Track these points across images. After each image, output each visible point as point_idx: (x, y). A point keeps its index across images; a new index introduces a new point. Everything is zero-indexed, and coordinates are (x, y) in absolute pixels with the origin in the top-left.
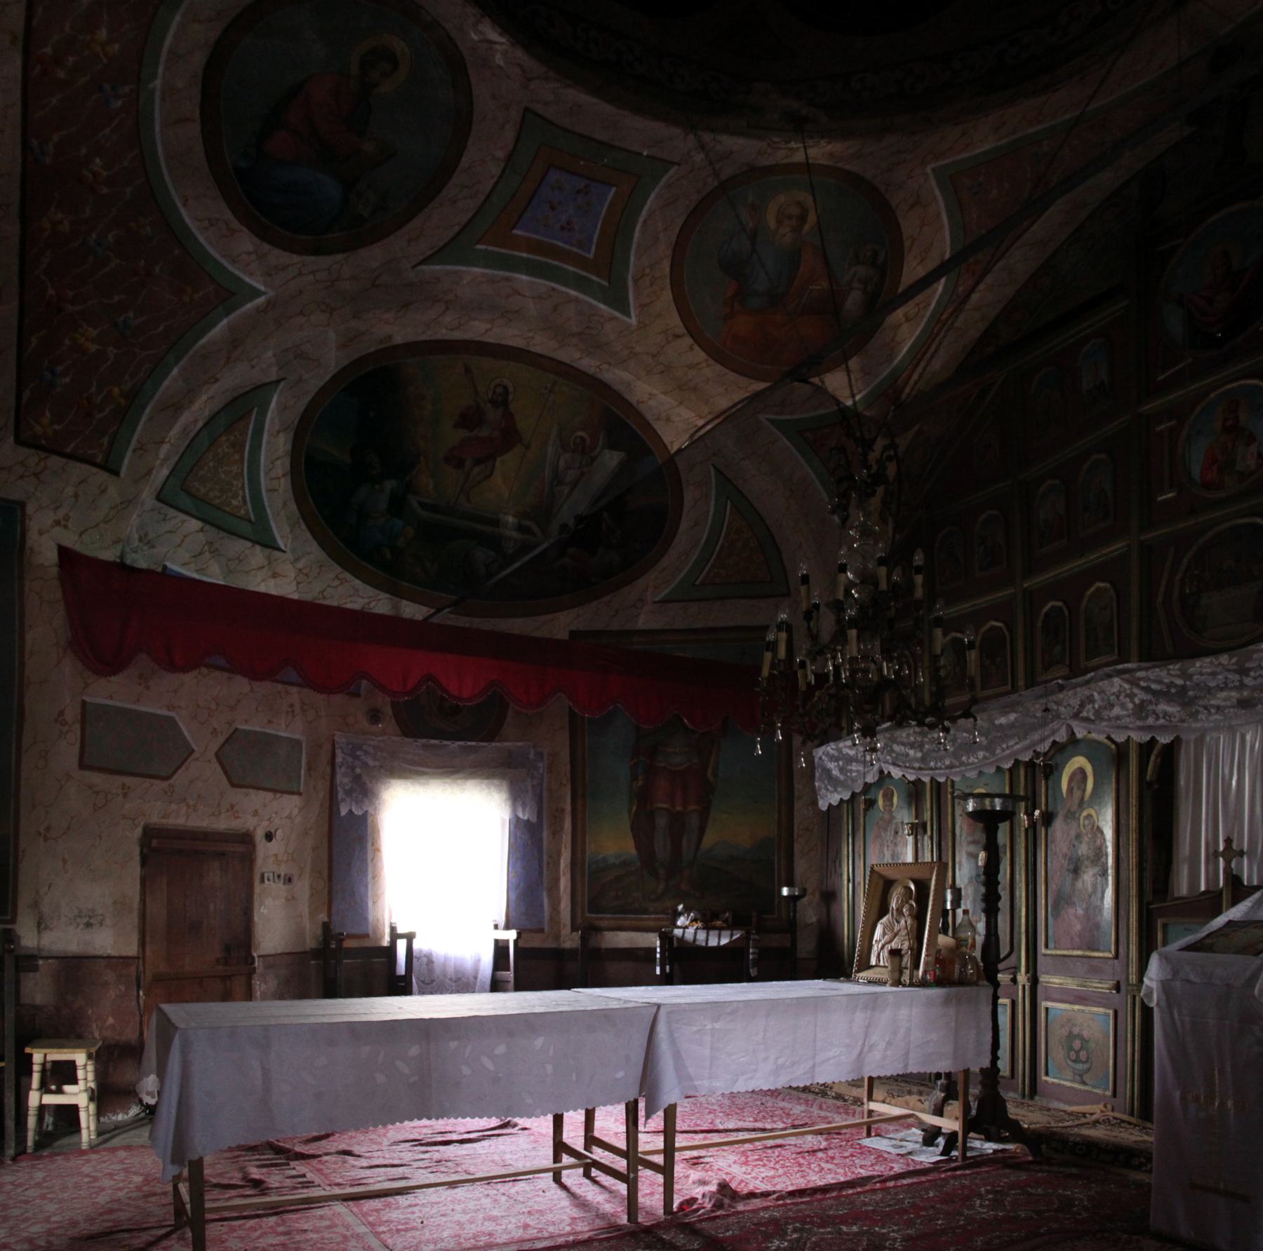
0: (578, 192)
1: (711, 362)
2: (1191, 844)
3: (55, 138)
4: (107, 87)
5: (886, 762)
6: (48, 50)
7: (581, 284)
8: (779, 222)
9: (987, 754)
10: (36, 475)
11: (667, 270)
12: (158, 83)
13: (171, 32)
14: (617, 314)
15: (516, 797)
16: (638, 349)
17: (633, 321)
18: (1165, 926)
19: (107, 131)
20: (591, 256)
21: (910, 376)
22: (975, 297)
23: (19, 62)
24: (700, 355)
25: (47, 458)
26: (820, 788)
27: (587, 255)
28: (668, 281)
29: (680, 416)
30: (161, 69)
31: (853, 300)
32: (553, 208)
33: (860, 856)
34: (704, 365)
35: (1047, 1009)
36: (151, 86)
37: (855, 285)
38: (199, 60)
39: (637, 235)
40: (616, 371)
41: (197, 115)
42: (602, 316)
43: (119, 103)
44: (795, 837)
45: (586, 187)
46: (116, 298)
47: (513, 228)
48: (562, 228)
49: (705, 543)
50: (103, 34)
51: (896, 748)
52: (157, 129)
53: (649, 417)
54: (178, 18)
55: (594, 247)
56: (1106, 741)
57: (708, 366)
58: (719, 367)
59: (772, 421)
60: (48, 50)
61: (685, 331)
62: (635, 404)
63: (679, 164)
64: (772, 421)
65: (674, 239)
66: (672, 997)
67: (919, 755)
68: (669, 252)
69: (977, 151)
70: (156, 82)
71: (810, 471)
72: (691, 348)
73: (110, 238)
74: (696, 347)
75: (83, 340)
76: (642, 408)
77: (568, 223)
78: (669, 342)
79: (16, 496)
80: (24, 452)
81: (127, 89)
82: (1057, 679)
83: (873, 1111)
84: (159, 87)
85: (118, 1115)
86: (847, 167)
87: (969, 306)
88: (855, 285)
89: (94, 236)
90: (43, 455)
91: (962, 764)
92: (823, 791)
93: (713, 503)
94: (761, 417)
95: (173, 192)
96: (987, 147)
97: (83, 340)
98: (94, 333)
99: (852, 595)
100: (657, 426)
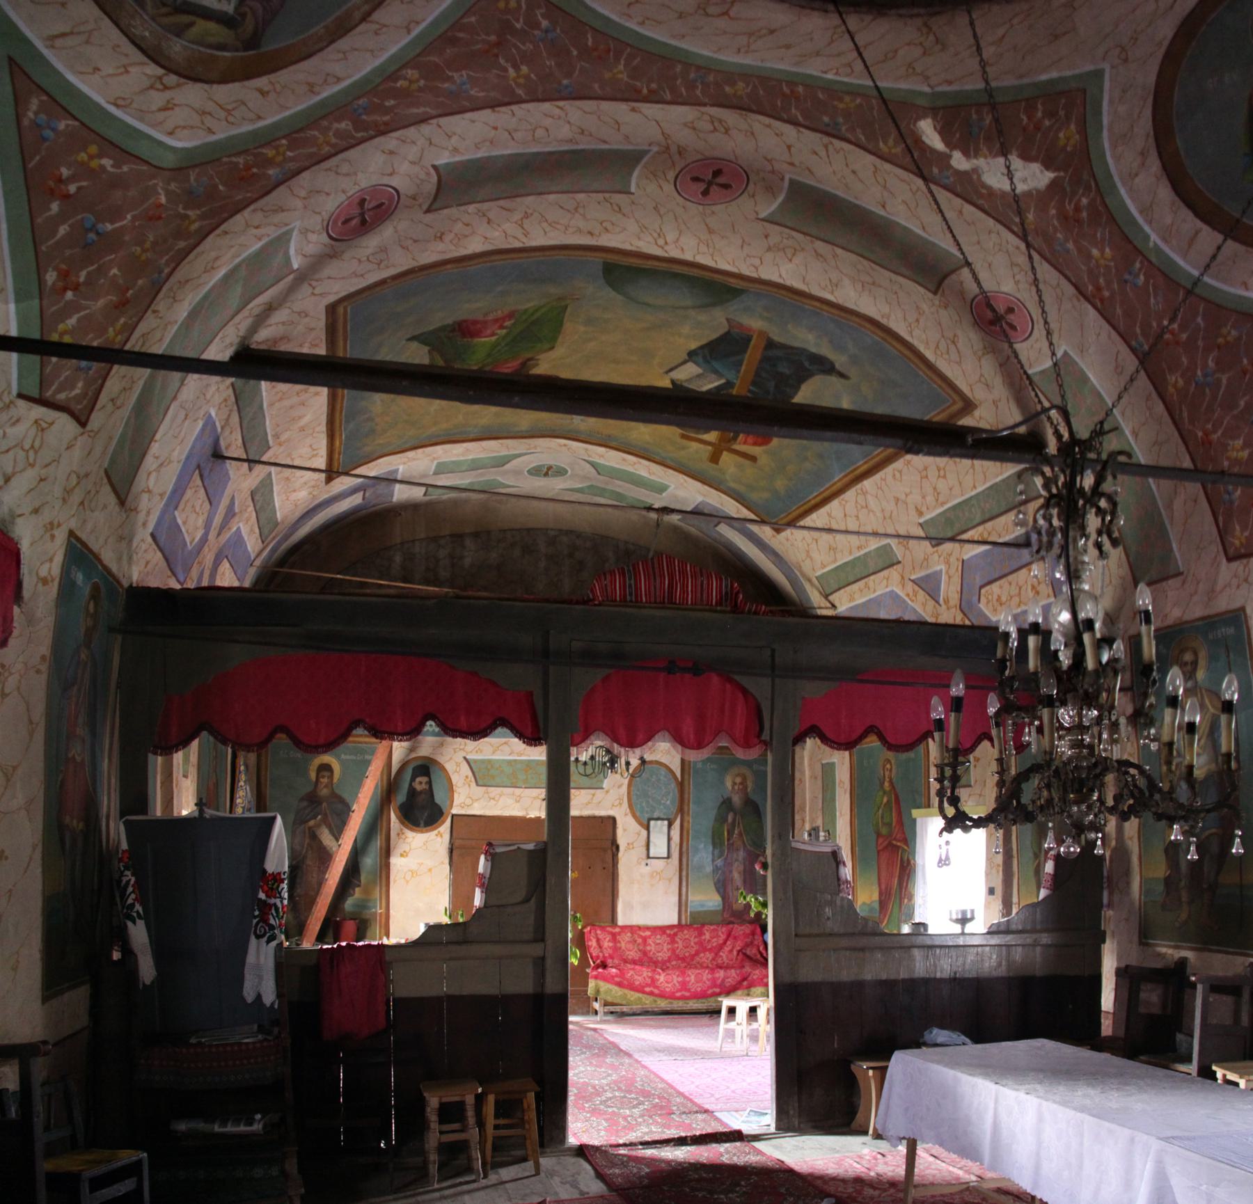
2: (163, 797)
3: (1138, 330)
4: (1127, 277)
6: (1090, 288)
10: (1246, 580)
12: (1154, 237)
13: (1128, 202)
15: (958, 827)
19: (1152, 300)
23: (1089, 307)
25: (1248, 562)
30: (1147, 228)
36: (1151, 244)
38: (1165, 193)
41: (1199, 224)
43: (1142, 277)
46: (1242, 403)
50: (1095, 252)
52: (1181, 263)
54: (1123, 191)
60: (1090, 288)
70: (1152, 239)
73: (1211, 364)
75: (1235, 453)
79: (1236, 605)
80: (1235, 565)
81: (1138, 265)
84: (1159, 242)
85: (375, 913)
89: (1199, 373)
90: (1245, 561)
95: (1232, 290)
97: (1235, 453)
98: (1239, 443)
99: (1075, 454)
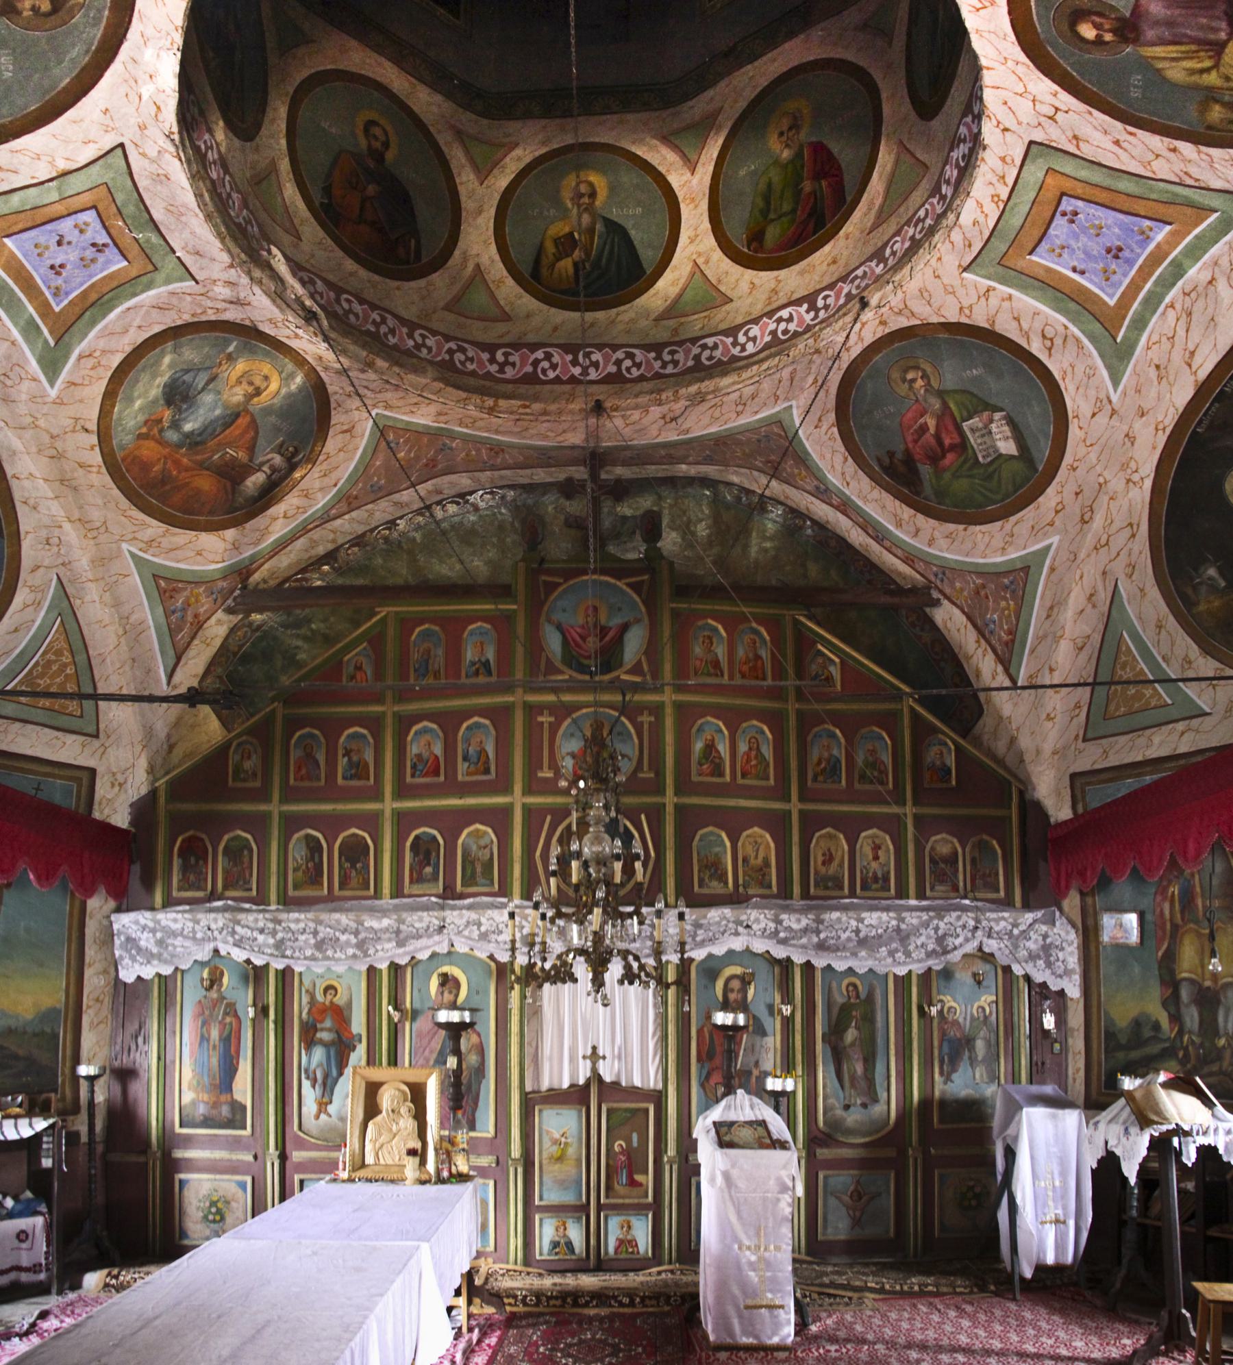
0: (94, 245)
1: (104, 470)
5: (226, 942)
7: (30, 330)
8: (239, 382)
9: (358, 953)
11: (115, 365)
14: (42, 378)
16: (41, 423)
17: (53, 393)
18: (540, 1111)
20: (57, 309)
21: (262, 565)
22: (339, 522)
24: (96, 458)
26: (121, 958)
27: (53, 304)
28: (109, 374)
29: (49, 509)
31: (256, 480)
32: (59, 243)
33: (174, 1032)
34: (95, 469)
35: (181, 1181)
37: (265, 468)
39: (112, 316)
40: (10, 434)
42: (27, 372)
44: (84, 1007)
45: (104, 245)
47: (8, 236)
48: (52, 267)
49: (18, 656)
51: (238, 929)
53: (17, 496)
55: (66, 302)
56: (488, 961)
57: (99, 472)
58: (107, 479)
59: (133, 555)
61: (95, 428)
62: (9, 476)
63: (197, 282)
64: (133, 555)
65: (140, 341)
66: (1024, 1188)
67: (271, 941)
68: (128, 349)
69: (414, 420)
71: (150, 617)
72: (92, 448)
74: (97, 449)
76: (14, 484)
77: (62, 266)
78: (74, 431)
82: (431, 895)
83: (469, 1276)
86: (322, 374)
87: (328, 526)
88: (265, 468)
91: (328, 958)
92: (127, 961)
93: (42, 613)
94: (125, 546)
96: (423, 421)
100: (21, 510)
